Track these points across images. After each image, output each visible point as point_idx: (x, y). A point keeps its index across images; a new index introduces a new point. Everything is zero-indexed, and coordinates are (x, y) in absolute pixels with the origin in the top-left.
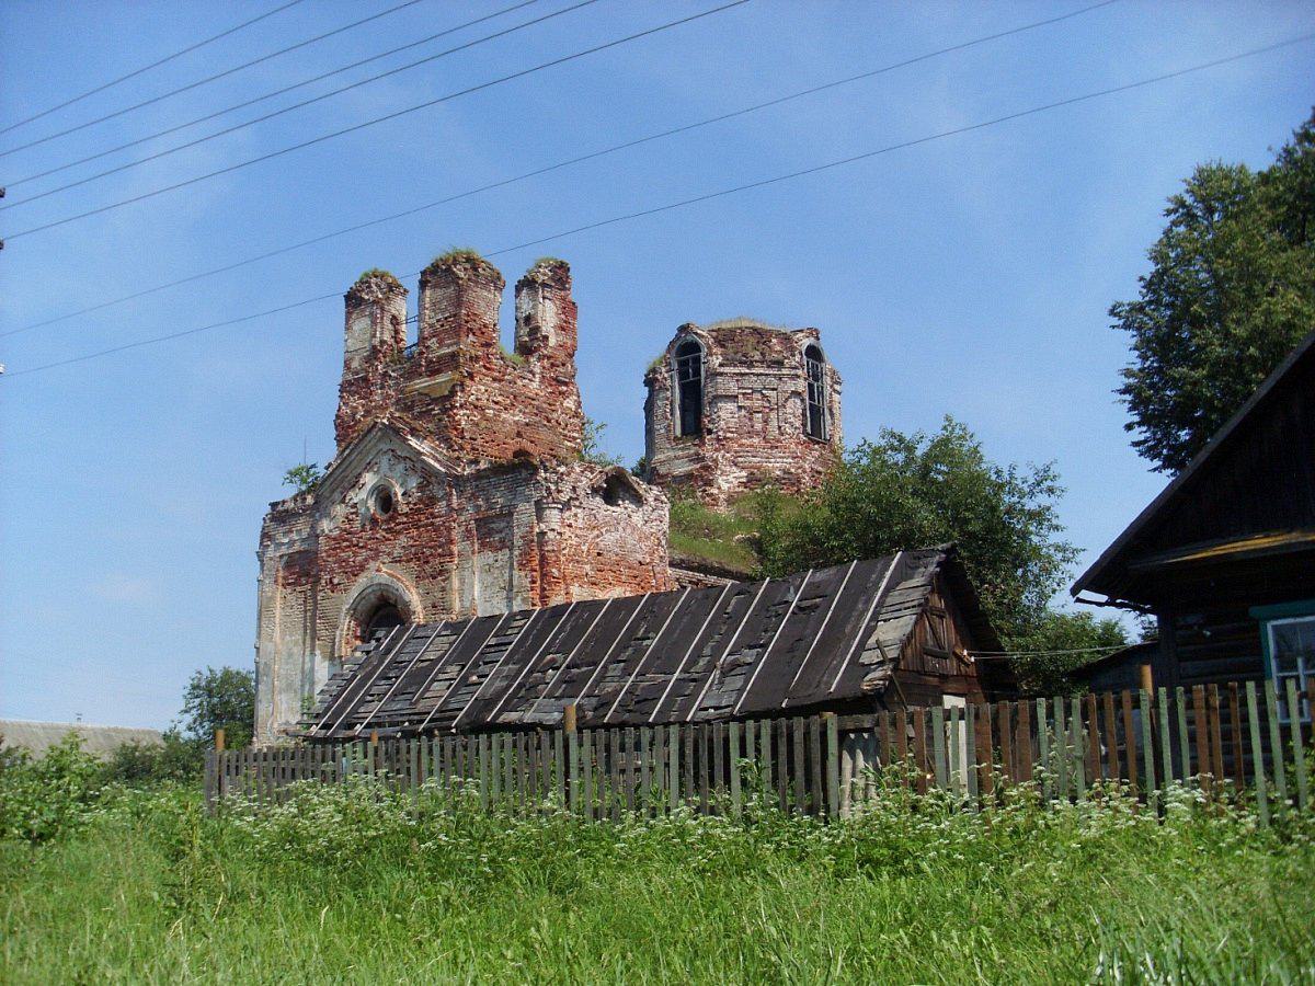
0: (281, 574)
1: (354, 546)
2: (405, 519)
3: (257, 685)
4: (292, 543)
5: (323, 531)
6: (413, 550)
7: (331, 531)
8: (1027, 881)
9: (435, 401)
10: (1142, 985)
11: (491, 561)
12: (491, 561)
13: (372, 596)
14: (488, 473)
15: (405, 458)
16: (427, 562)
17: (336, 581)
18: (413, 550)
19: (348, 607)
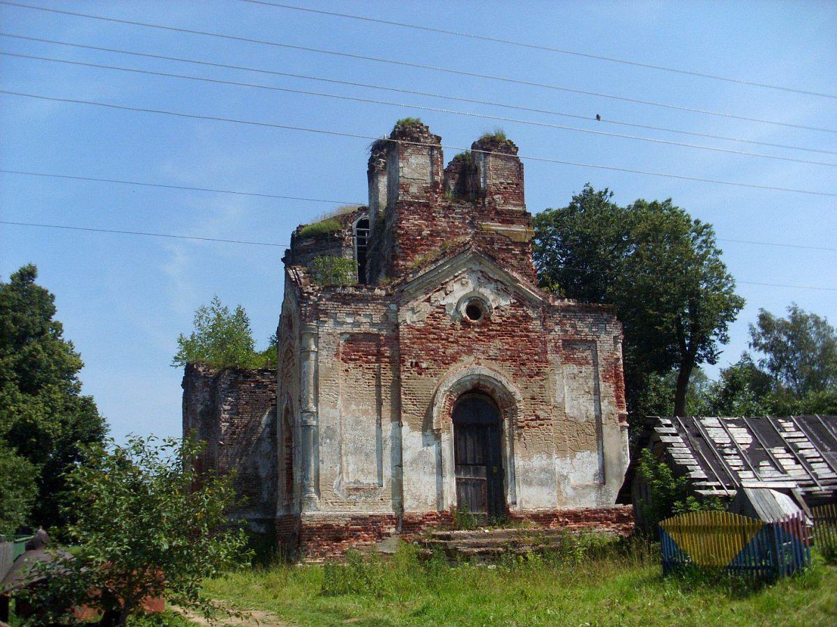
0: (341, 349)
1: (443, 339)
2: (499, 328)
3: (474, 449)
4: (356, 324)
5: (405, 321)
6: (509, 353)
7: (414, 322)
8: (181, 556)
9: (515, 244)
10: (836, 611)
11: (576, 371)
12: (576, 371)
13: (468, 383)
14: (576, 309)
15: (496, 281)
16: (524, 364)
17: (424, 365)
18: (509, 353)
19: (446, 389)
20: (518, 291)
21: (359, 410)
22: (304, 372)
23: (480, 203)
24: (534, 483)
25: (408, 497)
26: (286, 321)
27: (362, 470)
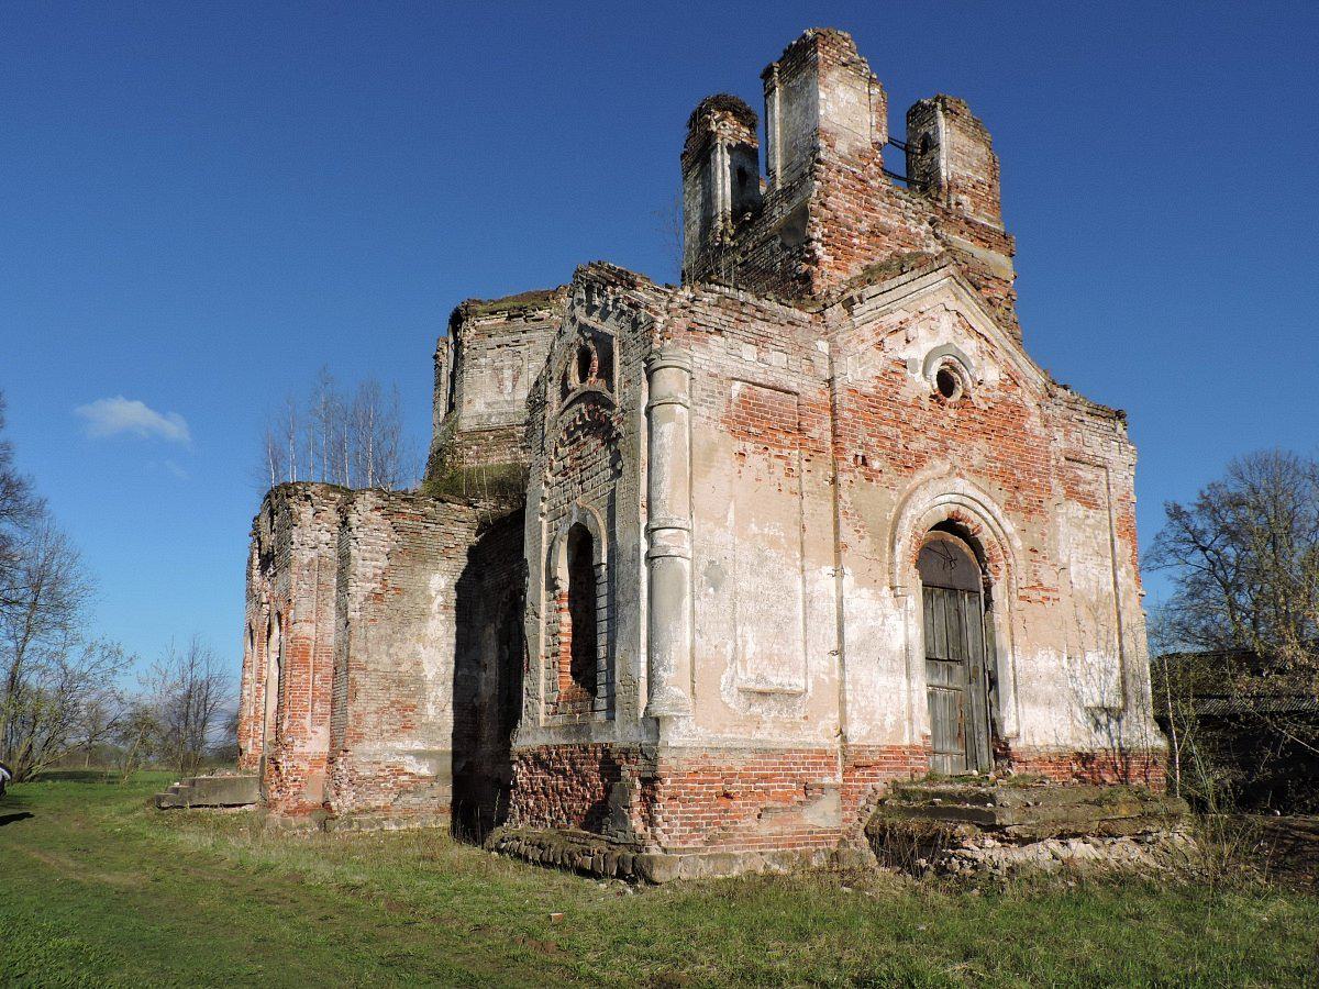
20: (1010, 361)
21: (763, 535)
22: (661, 446)
23: (436, 822)
24: (1040, 700)
25: (855, 715)
26: (607, 402)
27: (770, 657)
